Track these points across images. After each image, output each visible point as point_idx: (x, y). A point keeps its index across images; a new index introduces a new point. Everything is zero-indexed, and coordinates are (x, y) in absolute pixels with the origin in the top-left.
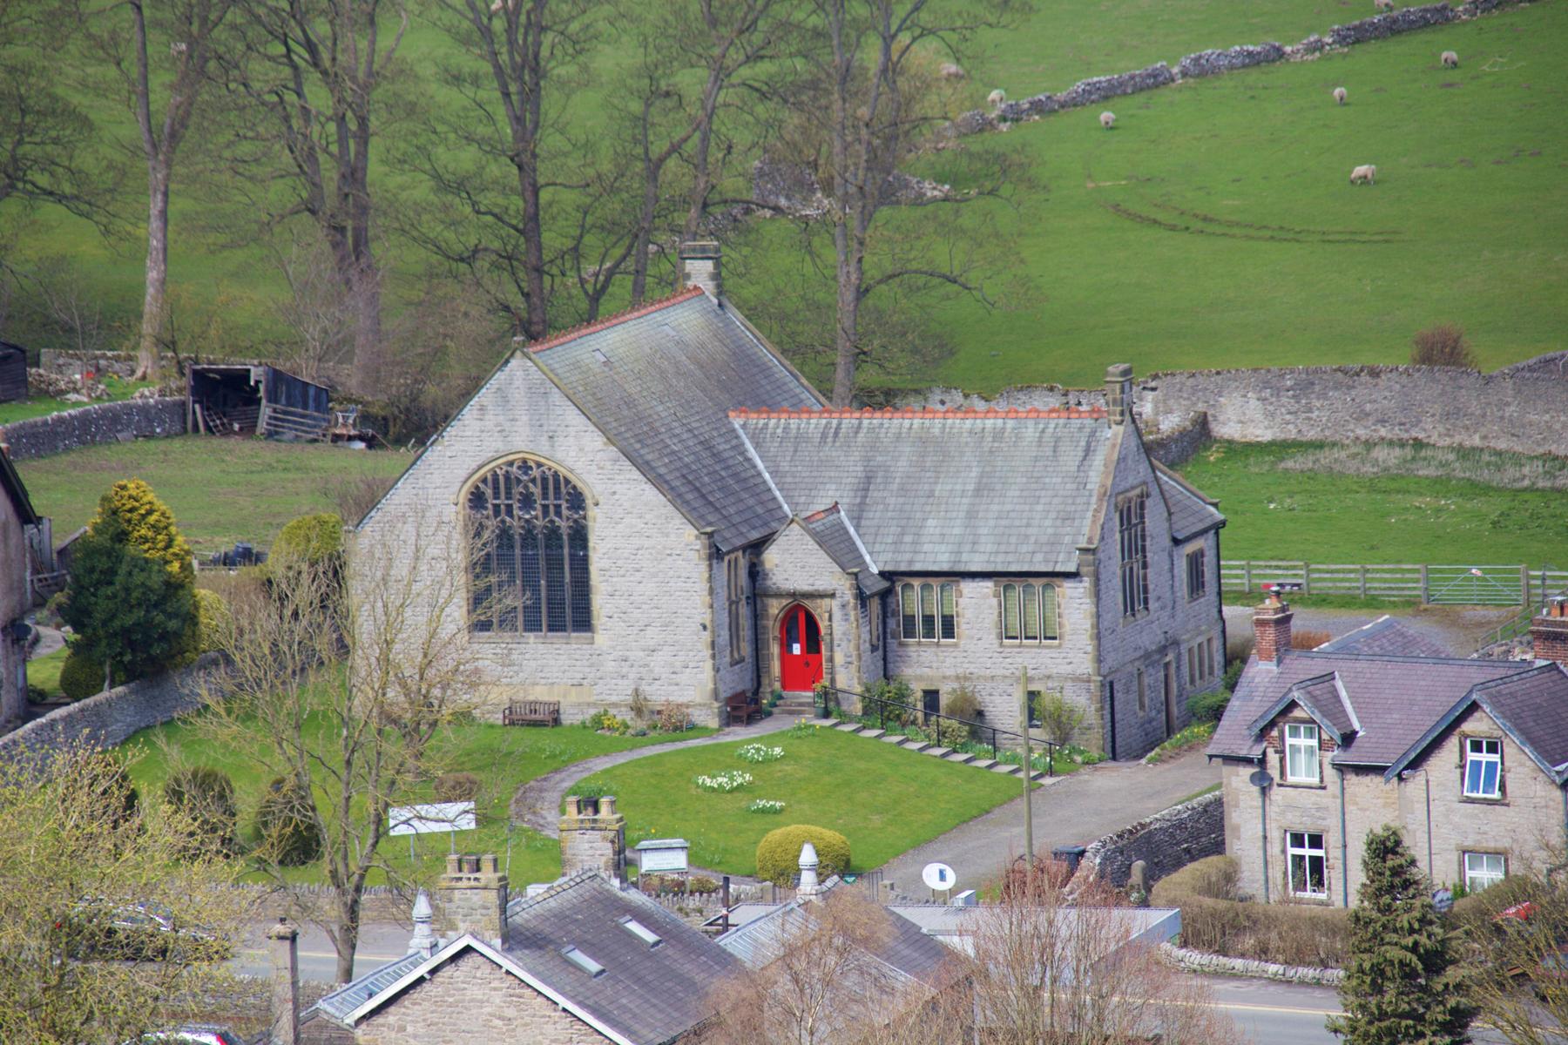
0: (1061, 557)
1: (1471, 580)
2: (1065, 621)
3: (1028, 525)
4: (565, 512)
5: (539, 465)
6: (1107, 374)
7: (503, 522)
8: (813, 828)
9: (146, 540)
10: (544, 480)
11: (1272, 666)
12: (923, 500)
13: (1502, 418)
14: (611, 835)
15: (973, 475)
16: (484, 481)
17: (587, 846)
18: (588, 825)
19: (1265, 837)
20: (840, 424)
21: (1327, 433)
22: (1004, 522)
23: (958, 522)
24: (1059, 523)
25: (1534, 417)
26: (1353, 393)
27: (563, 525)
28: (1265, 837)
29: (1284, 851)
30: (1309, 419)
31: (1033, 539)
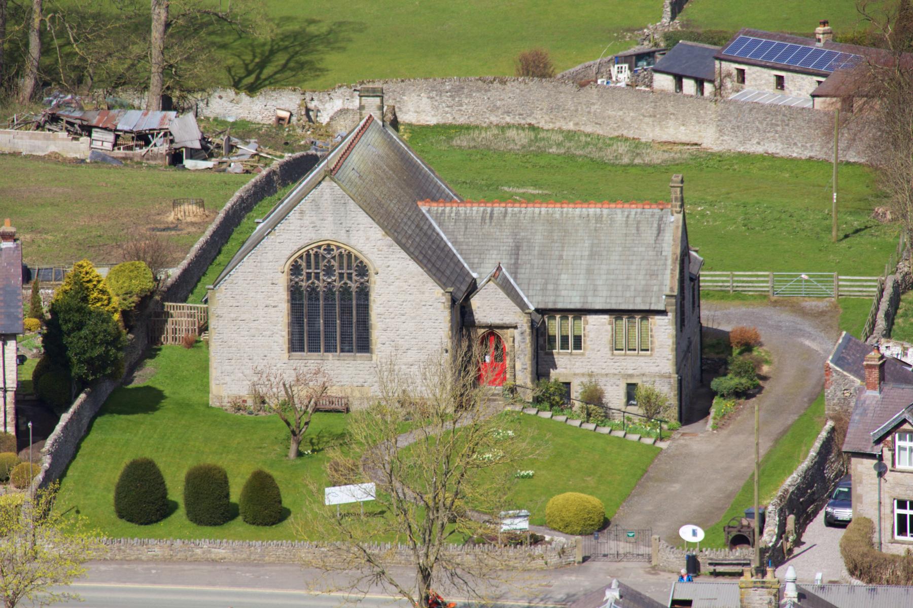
0: (653, 300)
1: (801, 281)
2: (655, 340)
3: (628, 279)
4: (354, 277)
5: (338, 248)
6: (671, 181)
7: (313, 283)
8: (582, 495)
9: (99, 300)
10: (341, 255)
11: (876, 393)
12: (556, 262)
13: (589, 112)
14: (775, 591)
15: (586, 245)
16: (301, 257)
17: (758, 598)
18: (759, 585)
19: (880, 503)
20: (492, 211)
21: (472, 119)
22: (612, 277)
23: (582, 276)
24: (648, 277)
25: (610, 113)
26: (489, 94)
27: (353, 286)
28: (880, 503)
29: (893, 512)
30: (461, 110)
31: (632, 288)
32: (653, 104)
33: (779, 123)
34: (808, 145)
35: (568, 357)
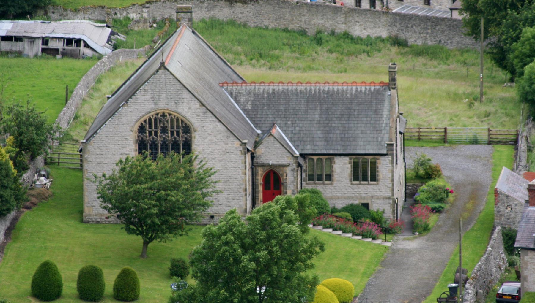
5: (170, 114)
7: (153, 138)
16: (145, 121)
32: (344, 15)
33: (429, 27)
34: (449, 42)
35: (322, 186)
